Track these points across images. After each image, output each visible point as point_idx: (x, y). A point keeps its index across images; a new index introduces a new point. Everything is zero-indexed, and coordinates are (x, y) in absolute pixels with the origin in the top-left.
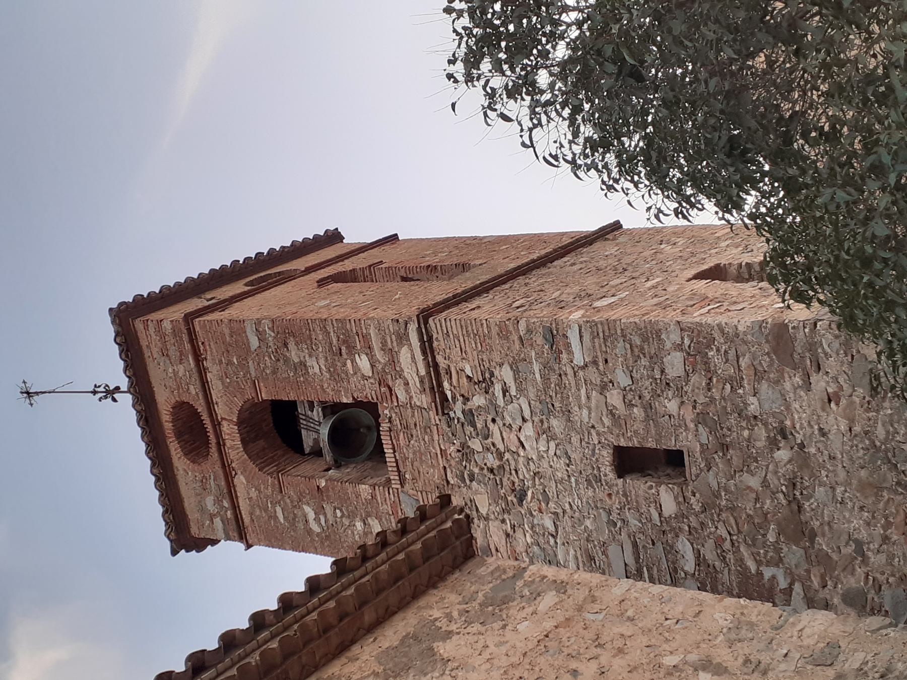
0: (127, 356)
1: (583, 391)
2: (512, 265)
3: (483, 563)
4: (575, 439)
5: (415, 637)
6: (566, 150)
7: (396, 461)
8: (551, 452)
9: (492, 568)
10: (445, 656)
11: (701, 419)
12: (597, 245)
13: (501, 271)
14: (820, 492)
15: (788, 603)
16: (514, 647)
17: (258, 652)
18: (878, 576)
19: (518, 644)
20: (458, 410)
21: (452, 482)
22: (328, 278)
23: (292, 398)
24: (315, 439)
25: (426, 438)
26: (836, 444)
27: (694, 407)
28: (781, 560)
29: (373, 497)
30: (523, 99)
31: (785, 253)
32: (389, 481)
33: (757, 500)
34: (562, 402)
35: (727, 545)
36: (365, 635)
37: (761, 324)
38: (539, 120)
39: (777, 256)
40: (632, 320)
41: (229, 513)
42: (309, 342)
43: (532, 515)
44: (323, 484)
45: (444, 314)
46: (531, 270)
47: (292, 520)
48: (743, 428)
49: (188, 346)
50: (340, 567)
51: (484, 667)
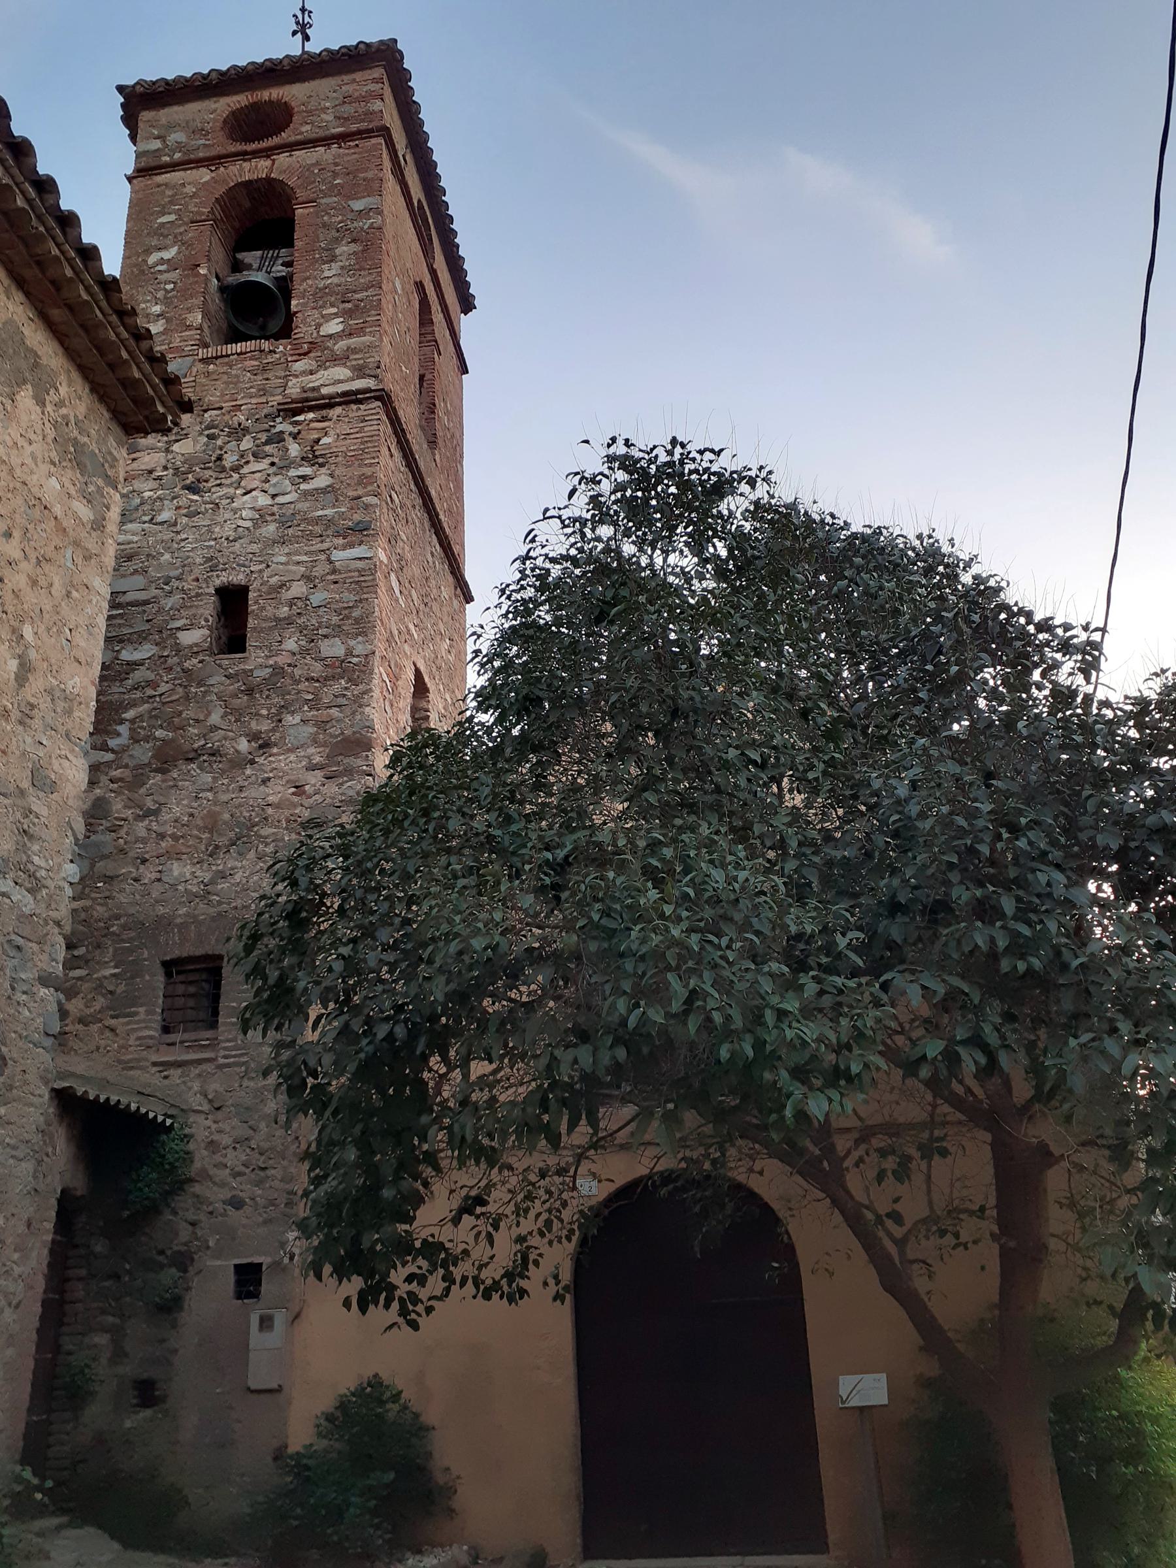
0: (343, 55)
1: (305, 558)
2: (433, 493)
3: (120, 444)
4: (255, 548)
5: (36, 365)
6: (539, 551)
7: (228, 356)
8: (241, 522)
9: (115, 453)
10: (18, 397)
11: (278, 671)
12: (450, 578)
13: (428, 481)
14: (208, 778)
15: (94, 747)
16: (32, 472)
17: (11, 183)
18: (125, 829)
19: (35, 477)
20: (283, 426)
21: (206, 415)
22: (425, 294)
23: (296, 243)
24: (251, 265)
25: (252, 390)
26: (255, 793)
27: (290, 665)
28: (138, 741)
29: (189, 327)
30: (588, 511)
31: (437, 747)
32: (206, 346)
33: (197, 721)
34: (294, 536)
35: (150, 692)
36: (36, 309)
37: (371, 728)
38: (568, 526)
39: (433, 738)
40: (377, 609)
41: (168, 159)
42: (357, 267)
43: (174, 498)
44: (202, 272)
45: (385, 418)
46: (429, 513)
47: (161, 232)
48: (269, 709)
49: (354, 127)
50: (110, 286)
51: (7, 438)
